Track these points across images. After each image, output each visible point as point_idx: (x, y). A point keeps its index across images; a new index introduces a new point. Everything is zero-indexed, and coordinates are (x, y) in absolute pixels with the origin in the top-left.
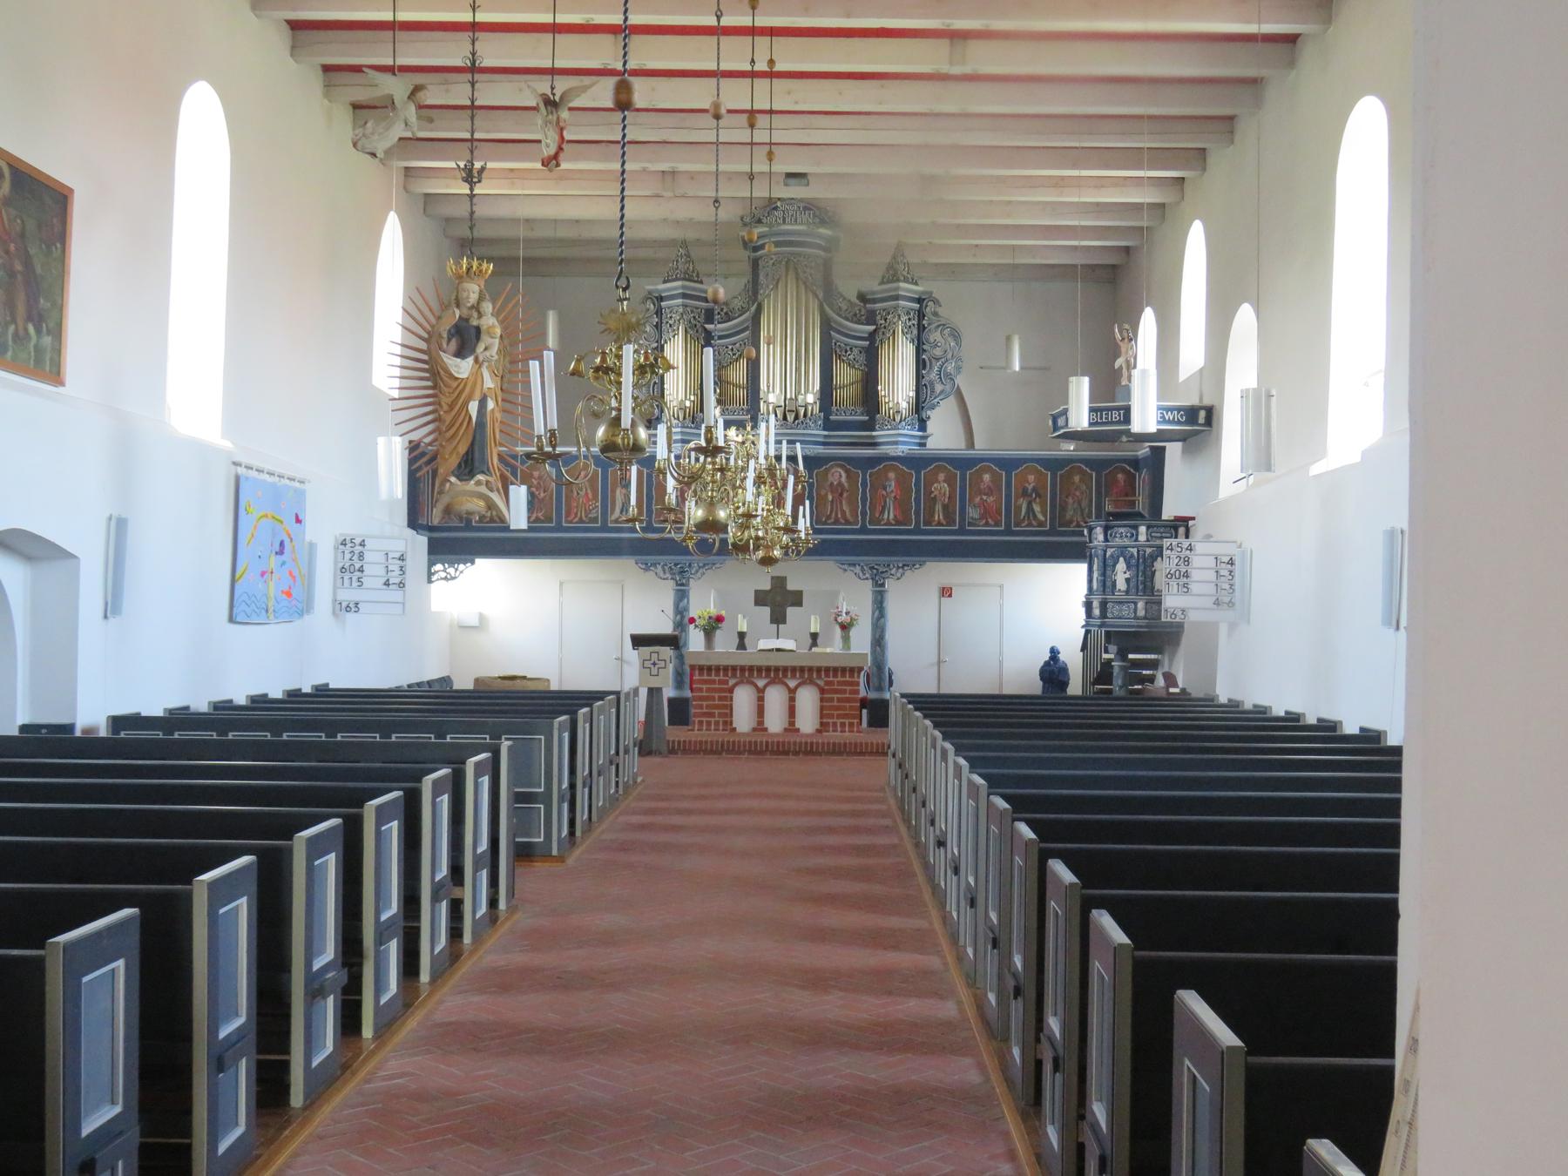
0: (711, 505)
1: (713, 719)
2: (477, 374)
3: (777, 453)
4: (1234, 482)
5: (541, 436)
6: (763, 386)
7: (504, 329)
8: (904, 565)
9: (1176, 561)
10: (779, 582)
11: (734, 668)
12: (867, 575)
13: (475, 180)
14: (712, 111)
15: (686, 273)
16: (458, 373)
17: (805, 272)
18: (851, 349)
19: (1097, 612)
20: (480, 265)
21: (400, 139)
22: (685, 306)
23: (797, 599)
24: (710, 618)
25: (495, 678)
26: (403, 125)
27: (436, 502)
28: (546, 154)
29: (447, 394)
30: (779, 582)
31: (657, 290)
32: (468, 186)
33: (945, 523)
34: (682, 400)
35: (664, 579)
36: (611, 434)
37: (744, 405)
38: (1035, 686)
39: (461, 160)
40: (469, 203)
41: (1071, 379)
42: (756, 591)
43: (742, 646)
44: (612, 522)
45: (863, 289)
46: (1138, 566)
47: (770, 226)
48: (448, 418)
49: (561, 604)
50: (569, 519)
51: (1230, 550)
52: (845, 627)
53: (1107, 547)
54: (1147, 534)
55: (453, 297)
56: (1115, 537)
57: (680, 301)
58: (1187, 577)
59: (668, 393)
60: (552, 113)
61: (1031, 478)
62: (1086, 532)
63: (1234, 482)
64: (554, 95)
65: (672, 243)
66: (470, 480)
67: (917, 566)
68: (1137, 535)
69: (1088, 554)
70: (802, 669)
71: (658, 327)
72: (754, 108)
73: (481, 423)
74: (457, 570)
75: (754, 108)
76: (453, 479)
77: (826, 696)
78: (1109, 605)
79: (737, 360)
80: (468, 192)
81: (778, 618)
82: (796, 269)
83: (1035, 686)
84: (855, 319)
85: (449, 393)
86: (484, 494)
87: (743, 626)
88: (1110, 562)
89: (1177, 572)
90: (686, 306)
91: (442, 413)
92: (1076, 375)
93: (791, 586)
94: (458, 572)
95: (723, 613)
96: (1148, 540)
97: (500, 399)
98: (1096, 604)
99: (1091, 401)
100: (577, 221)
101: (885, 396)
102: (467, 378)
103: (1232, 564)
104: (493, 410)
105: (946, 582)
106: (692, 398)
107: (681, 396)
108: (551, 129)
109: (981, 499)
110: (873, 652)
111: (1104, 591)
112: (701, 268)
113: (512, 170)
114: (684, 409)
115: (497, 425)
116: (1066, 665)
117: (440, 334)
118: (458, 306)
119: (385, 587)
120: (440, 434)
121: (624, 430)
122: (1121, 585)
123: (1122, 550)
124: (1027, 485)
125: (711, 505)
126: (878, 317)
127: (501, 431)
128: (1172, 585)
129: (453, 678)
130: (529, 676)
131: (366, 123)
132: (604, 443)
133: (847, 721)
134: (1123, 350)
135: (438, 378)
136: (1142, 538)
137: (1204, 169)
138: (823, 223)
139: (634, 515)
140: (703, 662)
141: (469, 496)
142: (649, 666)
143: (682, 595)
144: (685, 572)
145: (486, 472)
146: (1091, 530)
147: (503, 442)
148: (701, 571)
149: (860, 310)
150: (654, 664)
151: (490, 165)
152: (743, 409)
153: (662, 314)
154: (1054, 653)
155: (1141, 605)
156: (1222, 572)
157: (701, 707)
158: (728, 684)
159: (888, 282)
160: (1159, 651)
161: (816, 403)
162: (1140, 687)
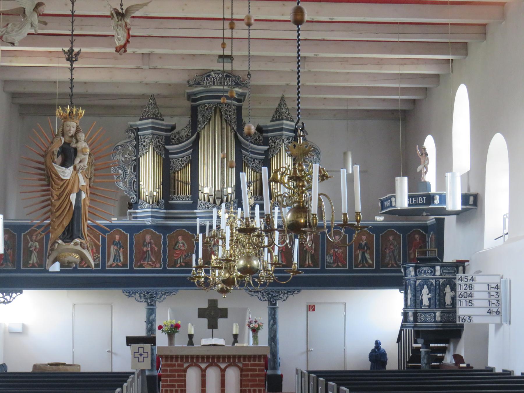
0: (248, 258)
1: (174, 389)
2: (75, 177)
3: (210, 224)
4: (495, 239)
5: (248, 218)
6: (201, 182)
7: (91, 150)
8: (288, 292)
9: (464, 287)
10: (213, 303)
11: (187, 357)
12: (266, 298)
13: (74, 59)
14: (246, 21)
15: (154, 114)
16: (64, 176)
17: (226, 114)
18: (254, 160)
19: (411, 319)
20: (78, 110)
21: (29, 34)
22: (153, 134)
23: (224, 313)
24: (172, 325)
25: (46, 365)
26: (30, 27)
27: (49, 256)
28: (117, 44)
29: (57, 189)
30: (213, 303)
31: (136, 125)
32: (70, 63)
33: (312, 266)
34: (151, 192)
35: (141, 302)
36: (295, 217)
37: (189, 194)
38: (366, 365)
39: (66, 47)
40: (70, 73)
41: (397, 178)
42: (199, 309)
43: (191, 343)
44: (108, 267)
45: (261, 124)
46: (436, 290)
47: (206, 86)
48: (58, 204)
49: (73, 317)
50: (81, 265)
51: (497, 280)
52: (255, 331)
53: (417, 279)
54: (441, 271)
55: (60, 130)
56: (421, 273)
57: (150, 131)
58: (471, 296)
59: (143, 187)
60: (121, 20)
61: (364, 238)
62: (402, 270)
63: (495, 239)
64: (122, 9)
65: (143, 96)
66: (71, 242)
67: (296, 292)
68: (435, 272)
69: (404, 283)
70: (229, 357)
71: (136, 147)
72: (233, 18)
73: (78, 207)
74: (11, 297)
75: (233, 18)
76: (60, 241)
77: (243, 373)
78: (419, 314)
79: (184, 167)
80: (69, 66)
81: (213, 326)
82: (221, 112)
83: (366, 365)
84: (256, 142)
85: (58, 189)
86: (80, 251)
87: (191, 331)
88: (418, 288)
89: (465, 294)
90: (154, 134)
91: (53, 201)
92: (400, 176)
93: (220, 306)
94: (12, 298)
95: (179, 322)
96: (441, 275)
97: (89, 193)
98: (410, 314)
99: (409, 191)
100: (85, 83)
101: (275, 189)
102: (70, 180)
103: (498, 288)
104: (85, 199)
105: (311, 302)
106: (157, 190)
107: (151, 189)
108: (121, 30)
109: (334, 251)
110: (270, 344)
111: (415, 306)
112: (162, 111)
113: (50, 52)
114: (152, 197)
115: (87, 208)
116: (385, 351)
117: (53, 152)
118: (63, 136)
119: (489, 314)
120: (52, 214)
121: (313, 215)
122: (426, 302)
123: (426, 281)
124: (361, 242)
125: (248, 258)
126: (270, 141)
127: (89, 212)
128: (462, 302)
129: (7, 364)
130: (67, 363)
131: (8, 24)
132: (291, 222)
133: (257, 389)
134: (422, 160)
135: (51, 179)
136: (438, 273)
137: (467, 54)
138: (237, 84)
139: (201, 264)
140: (168, 353)
141: (70, 252)
142: (142, 357)
143: (151, 311)
144: (153, 297)
145: (81, 237)
146: (405, 269)
147: (89, 218)
148: (163, 296)
149: (259, 137)
150: (141, 355)
151: (84, 50)
152: (188, 197)
153: (138, 139)
154: (378, 344)
155: (438, 314)
156: (492, 293)
157: (167, 381)
158: (183, 367)
159: (276, 120)
160: (447, 342)
161: (233, 193)
162: (438, 364)
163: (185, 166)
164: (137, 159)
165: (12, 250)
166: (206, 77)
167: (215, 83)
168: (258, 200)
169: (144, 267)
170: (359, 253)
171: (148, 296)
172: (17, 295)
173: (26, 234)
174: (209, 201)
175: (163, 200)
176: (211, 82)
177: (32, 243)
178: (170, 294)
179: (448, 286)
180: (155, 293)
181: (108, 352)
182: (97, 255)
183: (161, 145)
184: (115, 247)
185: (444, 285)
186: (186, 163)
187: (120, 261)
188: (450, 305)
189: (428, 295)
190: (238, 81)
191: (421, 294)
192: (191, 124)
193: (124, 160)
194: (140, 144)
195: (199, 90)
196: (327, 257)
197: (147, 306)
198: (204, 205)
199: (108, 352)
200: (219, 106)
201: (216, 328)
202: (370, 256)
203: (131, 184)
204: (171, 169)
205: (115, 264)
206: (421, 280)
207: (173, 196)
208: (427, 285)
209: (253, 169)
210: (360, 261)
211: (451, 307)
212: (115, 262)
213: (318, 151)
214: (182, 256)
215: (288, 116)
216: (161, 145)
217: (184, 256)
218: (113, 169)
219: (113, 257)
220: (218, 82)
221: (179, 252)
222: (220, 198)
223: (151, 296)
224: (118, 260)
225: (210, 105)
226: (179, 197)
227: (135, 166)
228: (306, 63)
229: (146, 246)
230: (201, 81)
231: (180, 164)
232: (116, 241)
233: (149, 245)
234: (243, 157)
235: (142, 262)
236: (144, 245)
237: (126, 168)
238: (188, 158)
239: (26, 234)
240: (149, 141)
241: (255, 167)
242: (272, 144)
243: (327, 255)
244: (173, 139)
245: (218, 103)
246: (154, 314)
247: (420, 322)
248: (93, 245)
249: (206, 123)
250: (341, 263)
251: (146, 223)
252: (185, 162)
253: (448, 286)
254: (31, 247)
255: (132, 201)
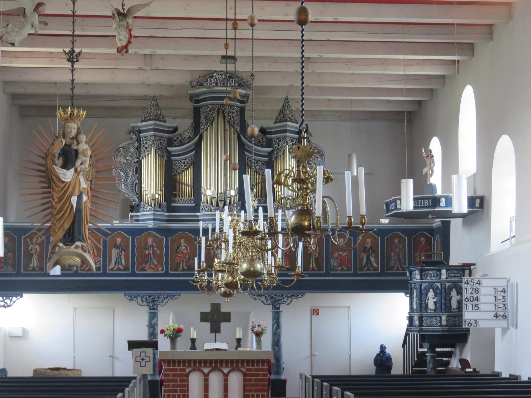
0: (252, 261)
1: (176, 394)
2: (76, 179)
3: (213, 227)
4: (502, 242)
5: (252, 221)
6: (203, 185)
7: (92, 152)
8: (292, 296)
9: (470, 291)
10: (216, 307)
11: (189, 361)
12: (269, 302)
13: (75, 60)
14: (249, 21)
15: (156, 116)
16: (65, 178)
17: (229, 116)
18: (257, 162)
19: (417, 323)
20: (79, 112)
21: (29, 34)
22: (155, 136)
23: (227, 317)
24: (174, 330)
25: (47, 369)
26: (30, 27)
27: (49, 259)
28: (119, 45)
29: (58, 192)
30: (216, 307)
31: (138, 127)
32: (71, 64)
33: (316, 269)
34: (153, 194)
35: (142, 306)
36: (299, 220)
37: (191, 197)
38: (371, 370)
39: (67, 47)
40: (71, 74)
41: (402, 180)
42: (201, 313)
43: (193, 347)
44: (109, 270)
45: (265, 126)
46: (441, 294)
47: (208, 87)
48: (58, 206)
49: (74, 322)
50: (83, 268)
51: (503, 283)
52: (258, 335)
53: (422, 282)
54: (446, 275)
55: (61, 132)
56: (427, 276)
57: (152, 133)
58: (477, 300)
59: (144, 189)
60: (122, 20)
61: (369, 241)
62: (408, 274)
63: (502, 242)
64: (124, 9)
65: (145, 98)
66: (72, 245)
67: (300, 296)
68: (441, 275)
69: (410, 287)
70: (232, 361)
71: (138, 149)
72: (236, 18)
73: (79, 210)
74: (11, 301)
75: (236, 18)
76: (61, 245)
77: (246, 378)
78: (424, 318)
79: (187, 169)
80: (70, 66)
81: (215, 330)
82: (224, 114)
83: (371, 370)
84: (259, 144)
85: (59, 191)
86: (81, 254)
87: (194, 335)
88: (424, 292)
89: (471, 297)
90: (156, 136)
91: (54, 203)
92: (405, 178)
93: (223, 309)
94: (12, 302)
95: (182, 326)
96: (447, 278)
97: (90, 195)
98: (416, 318)
99: (414, 194)
100: (86, 84)
101: (279, 191)
102: (70, 182)
103: (504, 292)
104: (86, 201)
105: (316, 306)
106: (160, 193)
107: (153, 191)
108: (123, 30)
109: (339, 254)
110: (273, 348)
111: (421, 310)
112: (164, 112)
113: (51, 53)
114: (154, 199)
115: (88, 211)
116: (390, 356)
117: (54, 154)
118: (64, 137)
119: (495, 318)
120: (52, 216)
121: (317, 217)
122: (431, 306)
123: (431, 285)
124: (366, 245)
125: (252, 261)
126: (274, 143)
127: (90, 214)
128: (469, 305)
129: (7, 369)
130: (68, 368)
131: (8, 25)
132: (295, 225)
133: (260, 394)
134: (428, 163)
135: (52, 182)
136: (444, 277)
137: (473, 55)
138: (240, 86)
139: (204, 267)
140: (170, 358)
141: (71, 255)
142: (144, 362)
143: (153, 315)
144: (156, 301)
145: (82, 240)
146: (411, 272)
147: (91, 221)
148: (166, 300)
149: (262, 139)
150: (143, 359)
151: (85, 50)
152: (191, 199)
153: (140, 141)
154: (383, 348)
155: (444, 318)
156: (499, 297)
157: (169, 386)
158: (185, 371)
159: (280, 122)
160: (453, 346)
161: (236, 195)
162: (444, 368)
163: (187, 168)
164: (139, 161)
165: (12, 253)
166: (209, 78)
167: (218, 84)
168: (261, 202)
169: (146, 270)
170: (364, 256)
171: (150, 299)
172: (18, 299)
173: (27, 237)
174: (212, 203)
175: (165, 203)
176: (214, 83)
177: (32, 247)
178: (172, 298)
179: (454, 289)
180: (157, 296)
181: (109, 356)
182: (99, 259)
183: (163, 147)
184: (117, 251)
185: (450, 289)
186: (188, 165)
187: (122, 264)
188: (456, 309)
189: (434, 298)
190: (241, 82)
191: (426, 297)
192: (194, 126)
193: (125, 162)
194: (142, 145)
195: (201, 91)
196: (332, 260)
197: (149, 309)
198: (206, 207)
199: (109, 356)
200: (222, 107)
201: (219, 332)
202: (375, 260)
203: (133, 186)
204: (174, 171)
205: (116, 268)
206: (426, 284)
207: (176, 199)
208: (433, 289)
209: (256, 171)
210: (365, 265)
211: (457, 311)
212: (117, 265)
213: (323, 153)
214: (184, 260)
215: (292, 118)
216: (163, 147)
217: (186, 259)
218: (114, 171)
219: (114, 260)
220: (221, 84)
221: (181, 255)
222: (223, 201)
223: (153, 300)
224: (120, 264)
225: (213, 107)
226: (181, 200)
227: (137, 168)
228: (310, 64)
229: (148, 249)
230: (204, 82)
231: (182, 166)
232: (118, 244)
233: (151, 248)
234: (246, 159)
235: (144, 265)
236: (145, 249)
237: (128, 170)
238: (190, 160)
239: (27, 237)
240: (151, 143)
241: (258, 169)
242: (275, 146)
243: (331, 258)
244: (175, 141)
245: (221, 105)
246: (156, 318)
247: (426, 326)
248: (94, 248)
249: (209, 124)
250: (345, 266)
251: (148, 226)
252: (188, 164)
253: (454, 289)
254: (31, 250)
255: (134, 204)
